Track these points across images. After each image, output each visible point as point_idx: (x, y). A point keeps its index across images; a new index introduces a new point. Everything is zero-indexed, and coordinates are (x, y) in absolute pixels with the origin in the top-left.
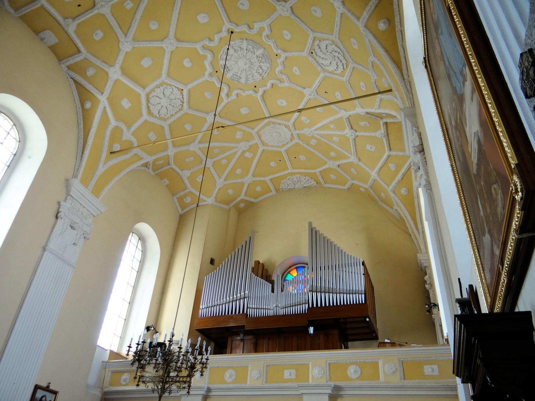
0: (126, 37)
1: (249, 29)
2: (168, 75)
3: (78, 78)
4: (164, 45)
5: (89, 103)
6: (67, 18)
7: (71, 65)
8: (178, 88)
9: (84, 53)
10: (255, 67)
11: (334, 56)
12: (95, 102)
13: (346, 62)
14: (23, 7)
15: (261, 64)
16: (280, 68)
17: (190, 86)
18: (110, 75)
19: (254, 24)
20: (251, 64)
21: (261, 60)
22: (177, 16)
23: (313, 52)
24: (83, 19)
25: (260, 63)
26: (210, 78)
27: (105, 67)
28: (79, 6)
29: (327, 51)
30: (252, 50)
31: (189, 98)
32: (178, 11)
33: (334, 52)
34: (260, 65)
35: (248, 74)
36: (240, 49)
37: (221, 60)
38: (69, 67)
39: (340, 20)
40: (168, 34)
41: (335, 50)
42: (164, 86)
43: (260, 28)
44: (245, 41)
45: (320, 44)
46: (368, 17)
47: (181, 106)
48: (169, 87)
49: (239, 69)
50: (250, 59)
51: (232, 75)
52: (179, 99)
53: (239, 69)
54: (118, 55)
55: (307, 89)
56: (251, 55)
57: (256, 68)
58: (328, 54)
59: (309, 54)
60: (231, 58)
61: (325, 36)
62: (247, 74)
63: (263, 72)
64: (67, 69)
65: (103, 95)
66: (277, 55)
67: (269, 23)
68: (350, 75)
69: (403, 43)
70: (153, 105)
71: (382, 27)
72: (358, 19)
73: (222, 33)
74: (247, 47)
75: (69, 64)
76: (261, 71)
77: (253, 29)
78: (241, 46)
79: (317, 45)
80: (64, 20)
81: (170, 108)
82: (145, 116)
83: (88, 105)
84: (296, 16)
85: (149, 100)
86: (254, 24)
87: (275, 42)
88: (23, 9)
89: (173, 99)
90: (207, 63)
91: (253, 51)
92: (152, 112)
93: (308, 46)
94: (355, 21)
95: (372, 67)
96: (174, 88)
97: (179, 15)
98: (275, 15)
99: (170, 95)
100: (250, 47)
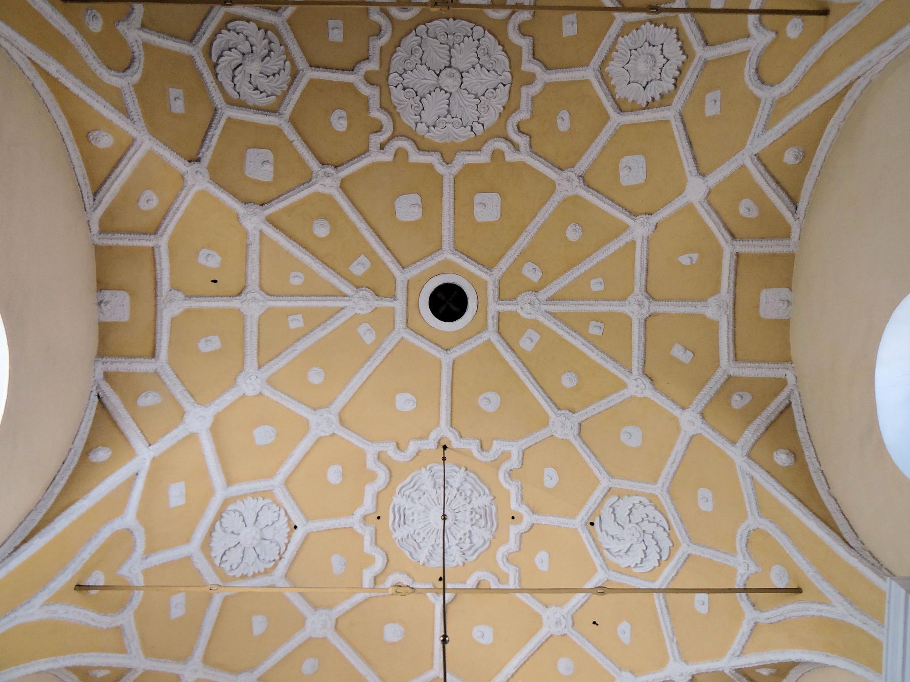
1: (480, 450)
2: (287, 482)
3: (114, 400)
4: (313, 418)
7: (117, 373)
8: (289, 520)
10: (459, 531)
11: (644, 531)
12: (124, 450)
13: (671, 545)
14: (119, 232)
16: (512, 545)
17: (315, 525)
18: (188, 419)
20: (454, 523)
21: (477, 520)
23: (597, 522)
25: (474, 527)
27: (186, 402)
28: (215, 281)
29: (630, 521)
30: (468, 493)
31: (295, 558)
32: (370, 371)
38: (107, 376)
39: (685, 451)
40: (331, 403)
42: (267, 501)
44: (463, 469)
45: (617, 504)
46: (753, 440)
47: (274, 563)
48: (275, 507)
49: (426, 526)
50: (456, 511)
51: (405, 536)
52: (278, 544)
53: (426, 526)
55: (553, 608)
56: (463, 502)
58: (628, 526)
59: (586, 524)
60: (420, 498)
61: (636, 486)
62: (437, 543)
63: (470, 548)
64: (102, 376)
65: (150, 448)
66: (513, 518)
68: (673, 575)
69: (830, 490)
70: (225, 531)
73: (427, 441)
74: (462, 484)
75: (116, 370)
77: (487, 451)
80: (171, 290)
81: (251, 556)
82: (193, 548)
83: (101, 455)
84: (584, 442)
85: (224, 515)
86: (495, 442)
87: (522, 488)
90: (370, 491)
91: (471, 495)
92: (211, 545)
93: (591, 504)
95: (746, 545)
96: (282, 513)
97: (368, 378)
99: (267, 525)
100: (467, 486)
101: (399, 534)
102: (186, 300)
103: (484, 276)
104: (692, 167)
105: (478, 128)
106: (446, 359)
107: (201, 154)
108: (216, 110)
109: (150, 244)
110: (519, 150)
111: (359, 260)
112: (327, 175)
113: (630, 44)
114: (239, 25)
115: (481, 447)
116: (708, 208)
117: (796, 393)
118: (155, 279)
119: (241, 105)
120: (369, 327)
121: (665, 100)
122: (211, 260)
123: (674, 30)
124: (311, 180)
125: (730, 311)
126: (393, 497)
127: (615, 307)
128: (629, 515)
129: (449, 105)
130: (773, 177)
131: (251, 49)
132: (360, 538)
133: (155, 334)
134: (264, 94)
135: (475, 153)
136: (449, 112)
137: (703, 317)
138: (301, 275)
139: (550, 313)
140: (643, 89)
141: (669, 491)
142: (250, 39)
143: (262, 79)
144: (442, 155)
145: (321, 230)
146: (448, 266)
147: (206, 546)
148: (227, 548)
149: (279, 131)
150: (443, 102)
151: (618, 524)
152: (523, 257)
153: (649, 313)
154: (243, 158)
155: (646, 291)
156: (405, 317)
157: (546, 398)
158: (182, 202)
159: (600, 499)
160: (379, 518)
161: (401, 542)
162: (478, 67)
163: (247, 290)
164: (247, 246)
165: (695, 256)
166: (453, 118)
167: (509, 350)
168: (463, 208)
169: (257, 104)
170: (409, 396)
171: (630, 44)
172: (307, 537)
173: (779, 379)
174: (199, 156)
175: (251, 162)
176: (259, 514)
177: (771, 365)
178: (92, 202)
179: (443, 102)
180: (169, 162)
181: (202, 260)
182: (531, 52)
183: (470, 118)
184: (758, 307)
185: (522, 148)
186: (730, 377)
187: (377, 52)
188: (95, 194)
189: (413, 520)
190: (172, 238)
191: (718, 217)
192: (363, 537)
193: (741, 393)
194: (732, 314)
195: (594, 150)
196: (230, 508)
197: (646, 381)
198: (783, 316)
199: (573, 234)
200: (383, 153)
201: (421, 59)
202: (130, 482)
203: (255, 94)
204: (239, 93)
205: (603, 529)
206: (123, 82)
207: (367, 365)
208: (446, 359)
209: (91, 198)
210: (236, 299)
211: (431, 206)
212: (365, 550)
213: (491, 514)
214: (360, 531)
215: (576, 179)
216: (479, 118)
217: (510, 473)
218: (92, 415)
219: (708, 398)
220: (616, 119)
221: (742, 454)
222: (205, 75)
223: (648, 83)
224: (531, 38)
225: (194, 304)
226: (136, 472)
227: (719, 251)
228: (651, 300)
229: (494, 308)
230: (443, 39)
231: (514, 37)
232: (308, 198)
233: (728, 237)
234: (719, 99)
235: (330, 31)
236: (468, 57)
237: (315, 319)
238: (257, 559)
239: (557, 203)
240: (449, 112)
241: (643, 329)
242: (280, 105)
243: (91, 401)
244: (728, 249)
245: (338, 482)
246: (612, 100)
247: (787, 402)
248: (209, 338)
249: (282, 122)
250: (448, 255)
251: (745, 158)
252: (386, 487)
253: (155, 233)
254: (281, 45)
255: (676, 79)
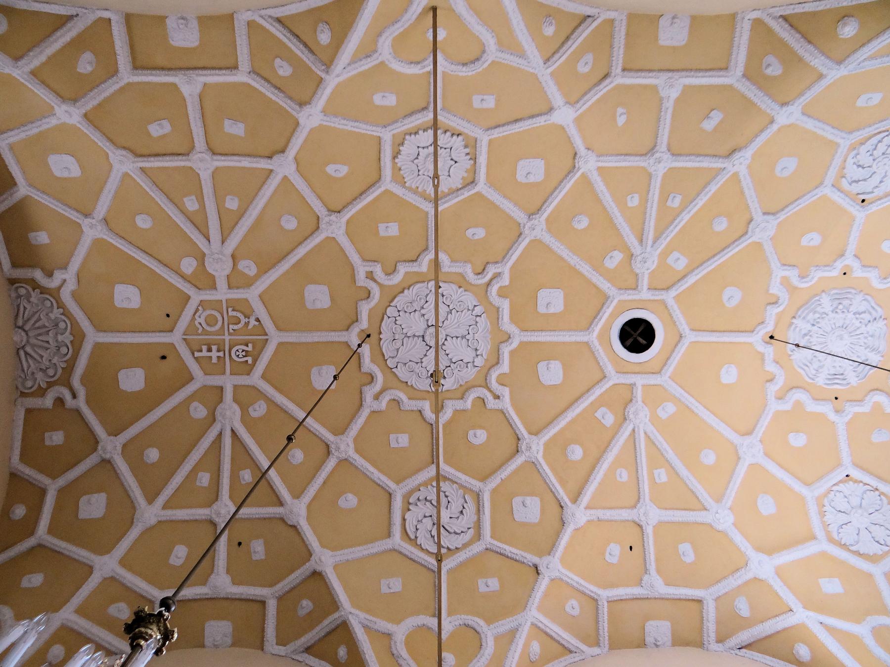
0: (709, 510)
1: (777, 305)
2: (807, 484)
3: (745, 636)
4: (747, 460)
5: (798, 647)
6: (641, 580)
7: (717, 632)
8: (841, 482)
9: (708, 595)
10: (853, 324)
11: (883, 154)
14: (598, 629)
15: (852, 309)
19: (771, 292)
22: (709, 413)
23: (863, 197)
24: (652, 557)
25: (850, 310)
26: (844, 414)
28: (631, 548)
29: (869, 167)
30: (817, 315)
32: (701, 408)
33: (875, 152)
34: (852, 313)
35: (865, 343)
36: (808, 337)
37: (816, 379)
38: (720, 640)
39: (815, 119)
41: (871, 148)
42: (826, 502)
43: (781, 284)
44: (794, 321)
46: (823, 58)
50: (834, 326)
51: (854, 374)
52: (865, 492)
54: (731, 541)
57: (857, 324)
58: (874, 168)
59: (862, 207)
60: (819, 360)
61: (837, 161)
62: (863, 344)
63: (870, 313)
64: (720, 645)
66: (845, 274)
67: (779, 265)
70: (857, 542)
71: (852, 29)
72: (821, 76)
73: (766, 355)
74: (808, 322)
76: (867, 317)
78: (803, 332)
79: (850, 184)
81: (877, 517)
84: (783, 210)
85: (843, 543)
86: (771, 292)
87: (817, 266)
88: (601, 632)
89: (861, 504)
91: (819, 313)
94: (824, 83)
96: (835, 488)
97: (708, 409)
98: (768, 248)
99: (848, 502)
100: (811, 317)
101: (853, 380)
102: (650, 574)
103: (615, 302)
104: (544, 118)
105: (478, 310)
106: (691, 337)
107: (529, 563)
108: (487, 549)
109: (606, 604)
110: (500, 273)
111: (600, 418)
112: (529, 448)
113: (413, 176)
114: (410, 530)
115: (773, 303)
116: (581, 102)
117: (771, 10)
118: (633, 599)
119: (478, 525)
120: (660, 408)
121: (471, 145)
122: (614, 553)
123: (407, 137)
124: (533, 463)
125: (676, 75)
126: (818, 385)
127: (656, 184)
128: (863, 168)
129: (457, 337)
130: (563, 44)
131: (428, 517)
132: (856, 414)
133: (680, 599)
134: (465, 506)
135: (500, 313)
136: (463, 337)
137: (677, 100)
138: (618, 471)
139: (654, 242)
140: (457, 164)
141: (849, 133)
142: (420, 519)
143: (453, 508)
144: (501, 343)
145: (576, 453)
146: (604, 336)
147: (873, 559)
148: (872, 540)
149: (494, 492)
150: (455, 343)
151: (870, 177)
152: (598, 267)
153: (667, 151)
154: (524, 524)
155: (646, 154)
156: (651, 375)
157: (734, 246)
158: (572, 579)
159: (841, 195)
160: (836, 398)
161: (859, 378)
162: (423, 312)
163: (637, 520)
164: (599, 520)
165: (620, 110)
166: (469, 333)
167: (685, 279)
168: (551, 323)
169: (474, 511)
170: (723, 371)
171: (413, 176)
172: (856, 465)
173: (752, 26)
174: (531, 565)
175: (526, 518)
176: (838, 510)
177: (737, 34)
178: (577, 654)
179: (458, 343)
180: (543, 592)
181: (614, 560)
182: (411, 264)
183: (469, 318)
184: (674, 48)
185: (499, 270)
186: (744, 76)
187: (413, 402)
188: (571, 652)
189: (840, 366)
190: (600, 586)
191: (589, 92)
192: (855, 413)
193: (764, 66)
194: (679, 73)
195: (507, 206)
196: (836, 537)
197: (737, 155)
198: (687, 23)
199: (582, 223)
200: (504, 396)
201: (417, 363)
202: (831, 630)
203: (467, 513)
204: (469, 528)
205: (871, 190)
206: (489, 633)
207: (696, 411)
208: (691, 337)
209: (574, 655)
210: (646, 530)
211: (548, 352)
212: (868, 411)
213: (839, 294)
214: (850, 417)
215: (532, 222)
216: (469, 310)
217: (802, 277)
218: (760, 655)
219: (766, 98)
220: (481, 186)
221: (836, 69)
222: (461, 559)
223: (452, 159)
224: (398, 264)
225: (652, 567)
226: (819, 624)
227: (619, 87)
228: (654, 151)
229: (645, 294)
230: (399, 343)
231: (397, 279)
232: (549, 465)
233: (608, 81)
234: (481, 97)
235: (401, 445)
236: (414, 320)
237: (658, 458)
238: (880, 511)
239: (552, 238)
240: (463, 337)
241: (681, 158)
242: (471, 490)
243: (746, 655)
244: (619, 80)
245: (805, 437)
246: (462, 191)
247: (780, 20)
248: (681, 553)
249: (486, 489)
250: (593, 337)
251: (545, 74)
252: (808, 391)
253: (596, 600)
254: (420, 490)
255: (453, 135)
